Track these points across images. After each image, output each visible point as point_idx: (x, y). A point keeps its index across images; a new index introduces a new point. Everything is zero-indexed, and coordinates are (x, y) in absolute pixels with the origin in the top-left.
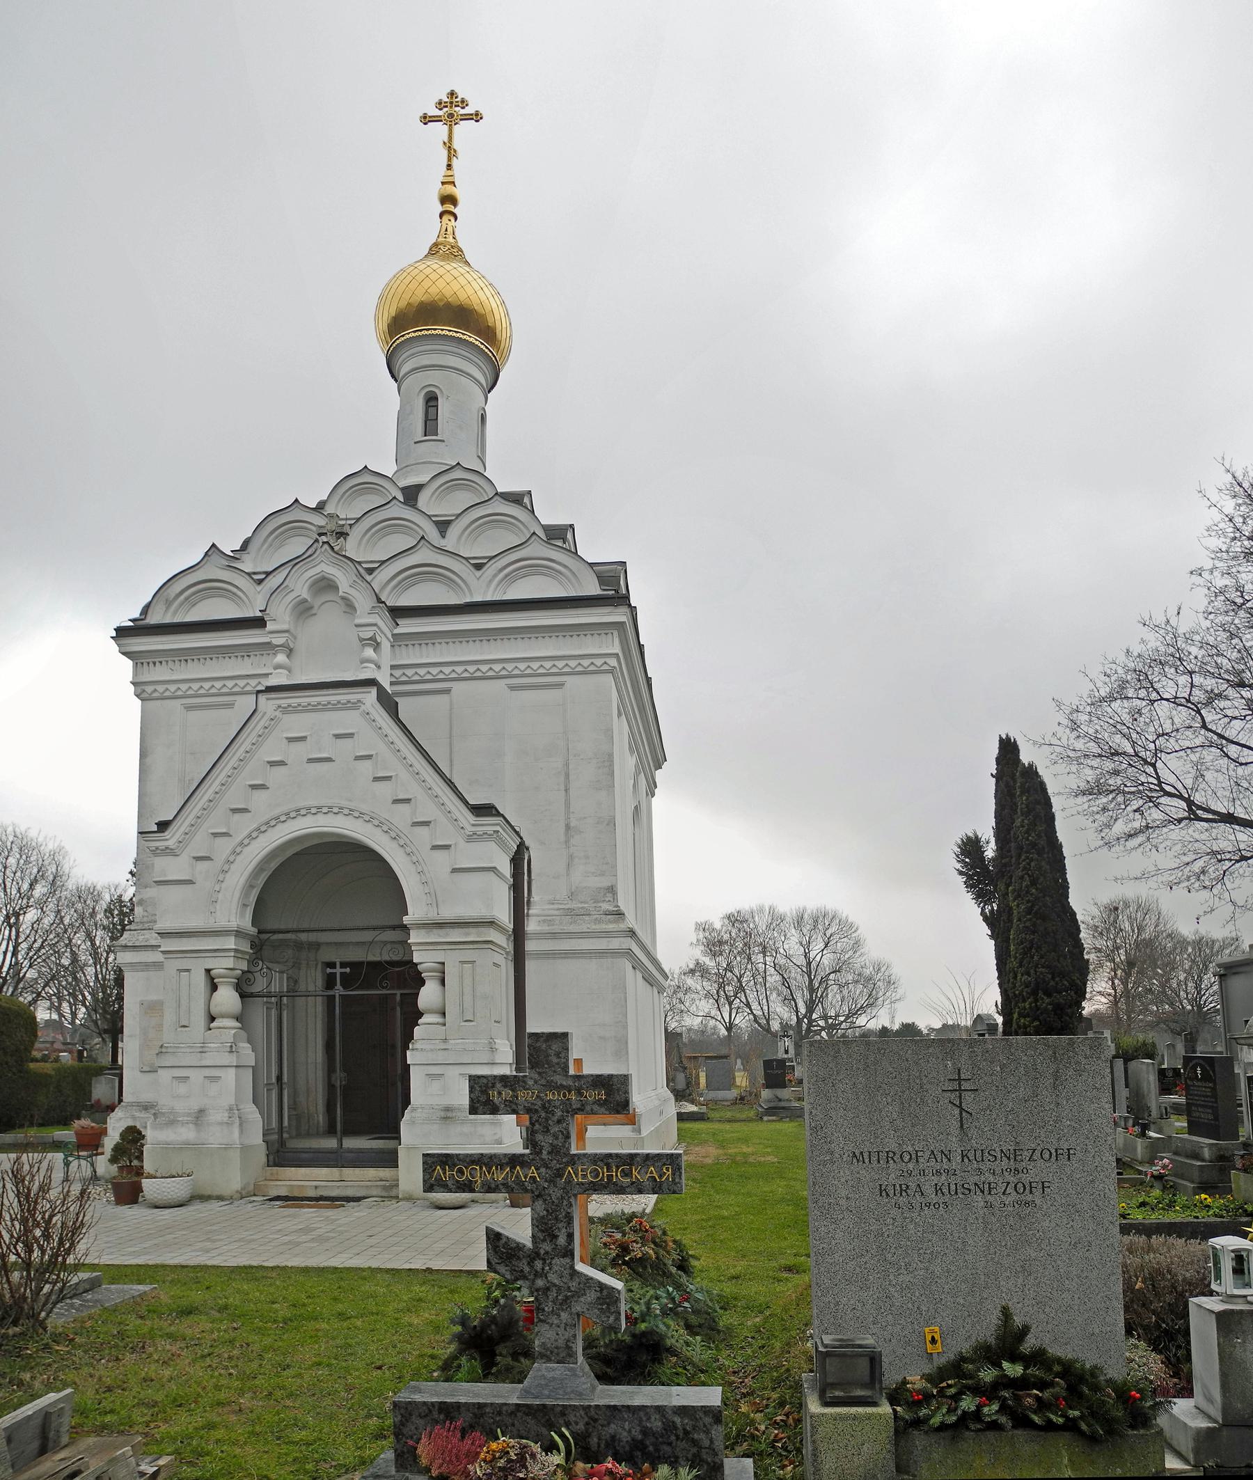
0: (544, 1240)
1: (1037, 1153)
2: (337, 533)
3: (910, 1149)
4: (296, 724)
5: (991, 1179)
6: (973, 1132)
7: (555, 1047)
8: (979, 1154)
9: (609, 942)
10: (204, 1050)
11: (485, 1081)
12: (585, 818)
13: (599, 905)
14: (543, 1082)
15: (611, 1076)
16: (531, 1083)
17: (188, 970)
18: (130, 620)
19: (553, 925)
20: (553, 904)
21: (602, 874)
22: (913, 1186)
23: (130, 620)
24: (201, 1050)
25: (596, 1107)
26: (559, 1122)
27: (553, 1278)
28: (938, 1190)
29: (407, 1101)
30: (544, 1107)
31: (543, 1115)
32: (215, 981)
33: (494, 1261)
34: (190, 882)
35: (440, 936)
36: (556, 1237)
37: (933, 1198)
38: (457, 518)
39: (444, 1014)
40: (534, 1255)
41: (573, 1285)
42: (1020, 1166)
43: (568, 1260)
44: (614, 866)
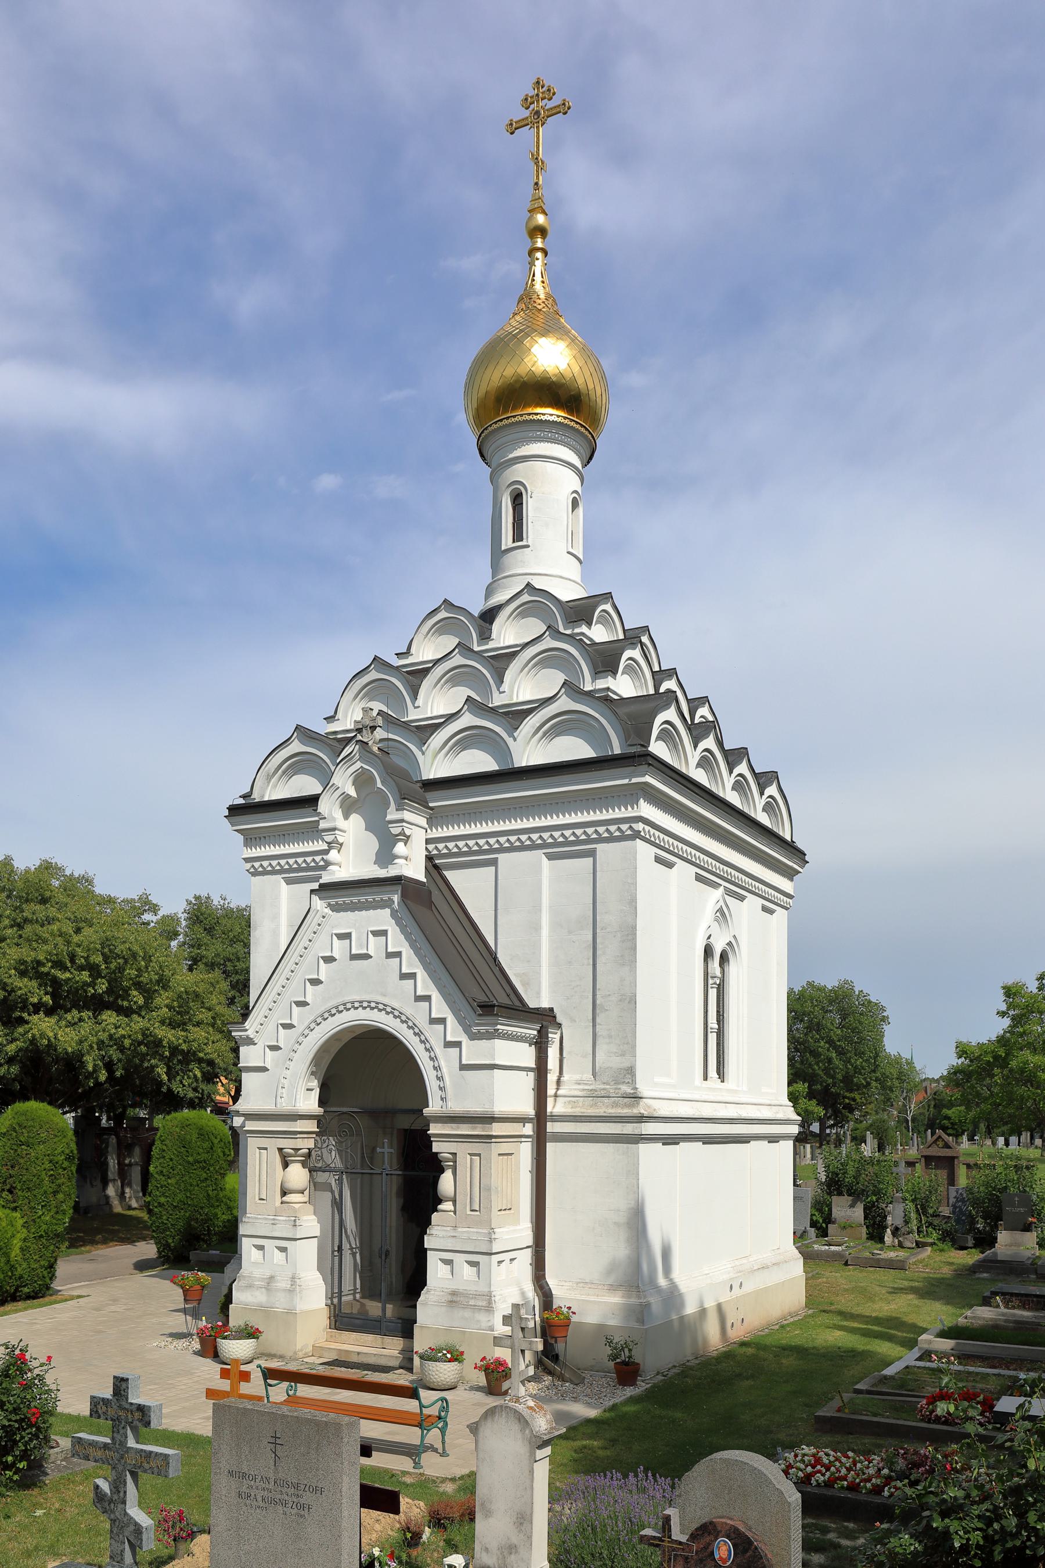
2: (370, 727)
3: (253, 1474)
4: (345, 921)
5: (286, 1498)
6: (280, 1468)
9: (623, 1126)
12: (609, 995)
13: (619, 1086)
14: (118, 1405)
16: (113, 1404)
17: (266, 1149)
18: (240, 797)
20: (579, 1084)
21: (623, 1055)
23: (240, 797)
24: (273, 1222)
29: (426, 1285)
32: (286, 1159)
34: (264, 1069)
36: (119, 1492)
37: (261, 1504)
44: (634, 1047)
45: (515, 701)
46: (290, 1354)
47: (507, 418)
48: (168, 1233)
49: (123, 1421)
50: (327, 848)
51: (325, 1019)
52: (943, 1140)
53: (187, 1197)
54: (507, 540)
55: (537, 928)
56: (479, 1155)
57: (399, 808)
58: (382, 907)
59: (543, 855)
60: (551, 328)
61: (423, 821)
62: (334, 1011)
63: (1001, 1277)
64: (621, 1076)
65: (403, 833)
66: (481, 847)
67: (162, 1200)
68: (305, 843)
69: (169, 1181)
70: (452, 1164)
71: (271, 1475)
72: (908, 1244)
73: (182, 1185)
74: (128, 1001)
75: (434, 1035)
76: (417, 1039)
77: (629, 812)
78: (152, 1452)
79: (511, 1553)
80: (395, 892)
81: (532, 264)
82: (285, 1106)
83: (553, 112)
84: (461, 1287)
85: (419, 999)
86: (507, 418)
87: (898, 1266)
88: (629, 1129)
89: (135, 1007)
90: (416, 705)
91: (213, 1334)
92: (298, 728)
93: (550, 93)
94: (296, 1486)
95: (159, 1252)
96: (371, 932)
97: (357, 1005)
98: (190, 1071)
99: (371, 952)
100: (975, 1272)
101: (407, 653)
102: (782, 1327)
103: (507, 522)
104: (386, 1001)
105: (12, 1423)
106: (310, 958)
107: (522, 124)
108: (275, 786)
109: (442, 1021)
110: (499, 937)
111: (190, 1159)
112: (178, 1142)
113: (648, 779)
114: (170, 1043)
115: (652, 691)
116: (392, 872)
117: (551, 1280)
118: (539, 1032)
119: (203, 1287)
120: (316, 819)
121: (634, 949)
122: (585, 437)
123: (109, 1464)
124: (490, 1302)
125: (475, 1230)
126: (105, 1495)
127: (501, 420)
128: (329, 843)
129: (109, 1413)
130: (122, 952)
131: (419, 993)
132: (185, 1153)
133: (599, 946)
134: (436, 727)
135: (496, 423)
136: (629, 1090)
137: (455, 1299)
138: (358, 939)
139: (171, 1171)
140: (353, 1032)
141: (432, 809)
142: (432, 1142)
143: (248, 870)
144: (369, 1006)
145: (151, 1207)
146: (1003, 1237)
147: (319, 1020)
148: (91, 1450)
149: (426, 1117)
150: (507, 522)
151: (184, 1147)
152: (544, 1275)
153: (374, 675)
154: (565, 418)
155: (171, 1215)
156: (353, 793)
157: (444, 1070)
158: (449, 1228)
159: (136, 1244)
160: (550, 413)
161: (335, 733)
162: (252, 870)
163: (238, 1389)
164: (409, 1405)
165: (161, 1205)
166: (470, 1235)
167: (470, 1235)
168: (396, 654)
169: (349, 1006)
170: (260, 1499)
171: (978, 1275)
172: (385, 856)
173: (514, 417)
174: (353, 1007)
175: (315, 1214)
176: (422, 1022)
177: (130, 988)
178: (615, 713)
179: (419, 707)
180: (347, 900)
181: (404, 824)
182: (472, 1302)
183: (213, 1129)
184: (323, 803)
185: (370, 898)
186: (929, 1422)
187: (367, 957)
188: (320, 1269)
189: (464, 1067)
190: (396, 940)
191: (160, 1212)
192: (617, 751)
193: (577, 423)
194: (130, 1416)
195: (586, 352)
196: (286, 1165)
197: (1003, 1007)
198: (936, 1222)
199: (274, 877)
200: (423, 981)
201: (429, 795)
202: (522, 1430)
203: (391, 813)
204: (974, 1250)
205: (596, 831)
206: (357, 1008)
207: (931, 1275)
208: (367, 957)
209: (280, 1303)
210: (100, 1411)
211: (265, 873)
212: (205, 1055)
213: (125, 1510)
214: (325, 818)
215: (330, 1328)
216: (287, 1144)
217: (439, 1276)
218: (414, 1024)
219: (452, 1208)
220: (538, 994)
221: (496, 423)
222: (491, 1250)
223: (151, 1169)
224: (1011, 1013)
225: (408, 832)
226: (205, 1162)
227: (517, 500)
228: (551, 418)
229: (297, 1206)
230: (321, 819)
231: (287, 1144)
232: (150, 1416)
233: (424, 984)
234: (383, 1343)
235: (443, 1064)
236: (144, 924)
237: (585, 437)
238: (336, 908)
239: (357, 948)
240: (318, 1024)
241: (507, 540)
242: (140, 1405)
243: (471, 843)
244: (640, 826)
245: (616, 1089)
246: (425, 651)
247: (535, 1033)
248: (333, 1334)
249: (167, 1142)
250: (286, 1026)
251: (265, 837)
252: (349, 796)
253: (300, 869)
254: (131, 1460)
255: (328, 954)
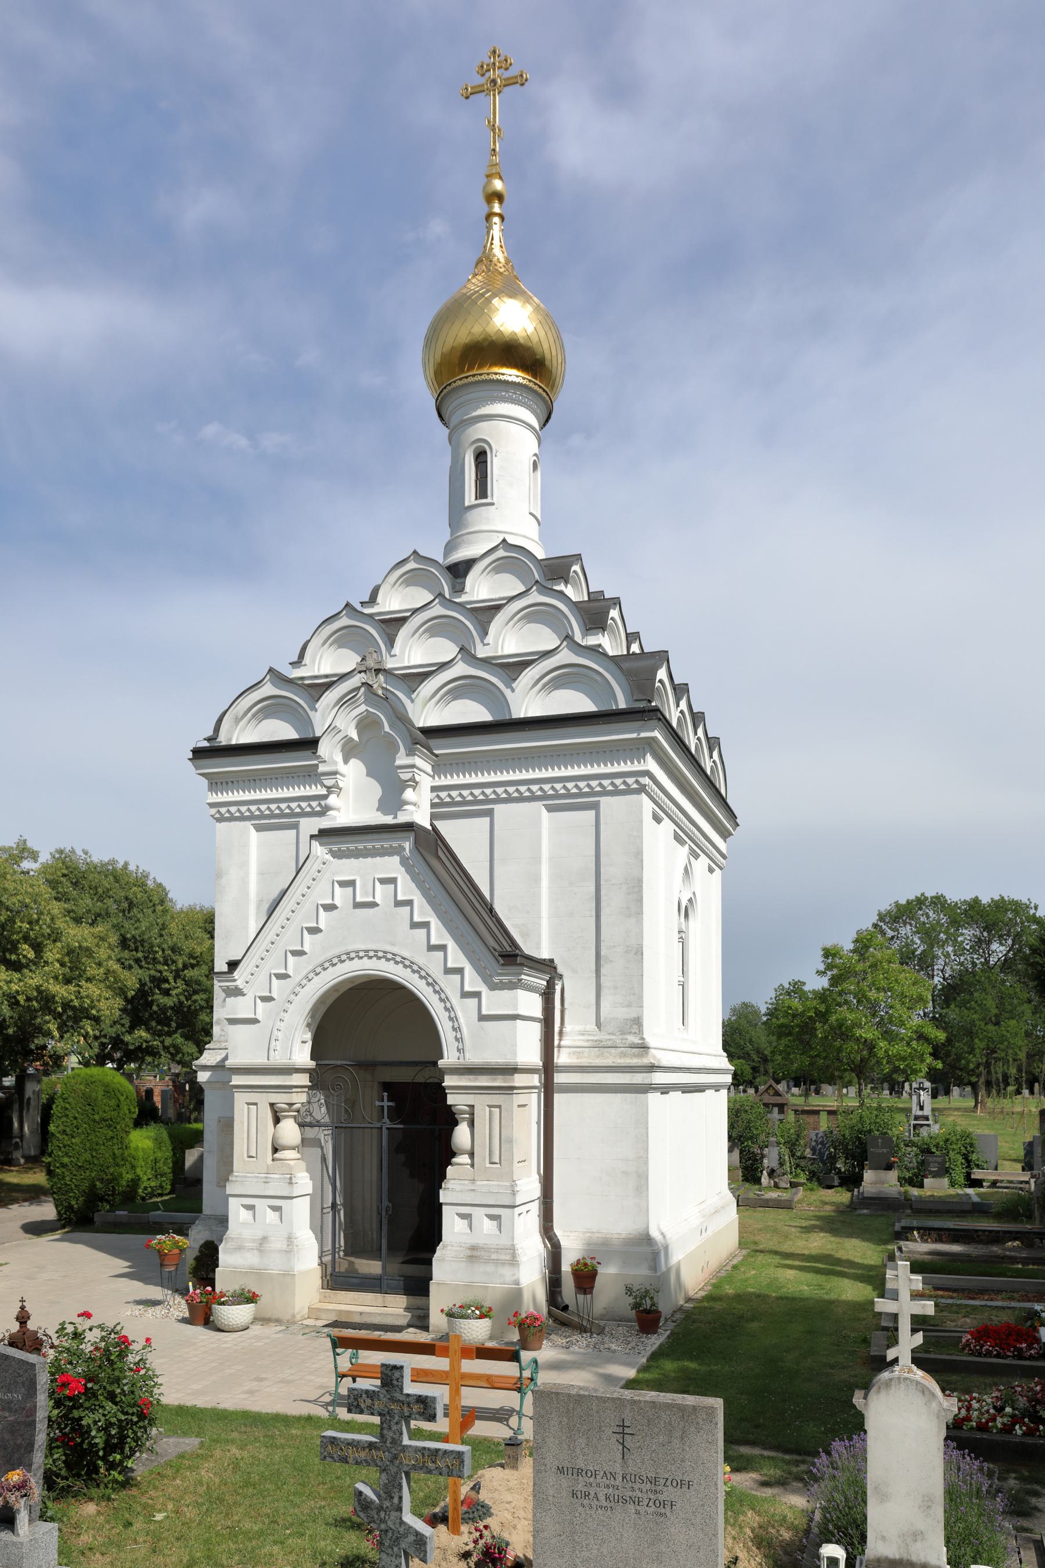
0: (386, 1499)
1: (669, 1482)
3: (592, 1469)
5: (640, 1495)
6: (630, 1462)
7: (397, 1374)
8: (633, 1477)
10: (268, 1180)
11: (356, 1392)
12: (614, 946)
14: (389, 1396)
15: (427, 1397)
16: (382, 1396)
17: (256, 1104)
18: (205, 739)
19: (582, 1058)
20: (583, 1035)
21: (629, 1006)
22: (592, 1494)
23: (205, 739)
24: (265, 1180)
25: (417, 1416)
26: (397, 1423)
27: (390, 1524)
28: (607, 1498)
29: (440, 1240)
30: (388, 1413)
31: (388, 1418)
33: (358, 1509)
34: (254, 1021)
35: (470, 1080)
36: (392, 1498)
38: (507, 603)
39: (473, 1154)
40: (380, 1508)
41: (401, 1529)
42: (659, 1488)
43: (399, 1514)
45: (500, 653)
46: (288, 1317)
47: (474, 376)
48: (71, 1194)
49: (396, 1416)
50: (326, 793)
51: (325, 969)
52: (774, 1089)
53: (93, 1157)
54: (470, 497)
55: (537, 879)
56: (499, 1107)
57: (410, 753)
58: (391, 854)
59: (543, 807)
60: (512, 290)
61: (428, 768)
62: (335, 961)
63: (880, 1213)
64: (628, 1027)
65: (413, 779)
66: (476, 797)
67: (66, 1160)
68: (224, 793)
69: (74, 1141)
70: (467, 1116)
71: (618, 1469)
72: (782, 1185)
73: (88, 1145)
74: (16, 954)
75: (450, 985)
76: (431, 989)
77: (636, 767)
78: (439, 1450)
79: (916, 1541)
80: (407, 839)
81: (489, 228)
82: (278, 1059)
83: (510, 82)
84: (480, 1241)
85: (432, 948)
86: (474, 376)
87: (785, 1205)
88: (638, 1078)
89: (24, 961)
90: (392, 653)
91: (205, 1300)
92: (271, 670)
93: (506, 65)
94: (654, 1481)
95: (59, 1213)
96: (378, 879)
97: (361, 954)
98: (81, 1028)
99: (378, 900)
100: (856, 1209)
101: (373, 599)
102: (735, 1267)
103: (470, 479)
104: (395, 950)
105: (130, 1417)
106: (308, 906)
107: (478, 90)
108: (243, 729)
109: (460, 971)
110: (496, 887)
111: (97, 1117)
112: (82, 1100)
113: (656, 734)
114: (63, 998)
115: (625, 653)
116: (402, 818)
117: (558, 1231)
118: (548, 982)
119: (181, 1250)
120: (316, 762)
121: (640, 901)
122: (543, 399)
123: (377, 1466)
124: (514, 1255)
125: (495, 1183)
126: (372, 1502)
127: (467, 377)
128: (328, 788)
129: (376, 1407)
130: (14, 904)
131: (433, 942)
132: (90, 1111)
133: (603, 898)
134: (328, 686)
135: (461, 379)
136: (637, 1041)
137: (474, 1254)
138: (363, 886)
139: (75, 1130)
140: (353, 982)
141: (437, 756)
142: (446, 1094)
143: (212, 816)
144: (357, 956)
145: (52, 1168)
146: (868, 1175)
147: (319, 970)
148: (350, 1452)
149: (440, 1069)
150: (470, 479)
151: (89, 1105)
152: (552, 1226)
153: (344, 621)
154: (530, 381)
155: (75, 1175)
156: (354, 736)
157: (462, 1020)
158: (466, 1182)
159: (10, 1207)
160: (512, 374)
161: (302, 678)
162: (217, 816)
163: (459, 1367)
164: (506, 1369)
165: (63, 1165)
166: (489, 1188)
167: (489, 1188)
168: (361, 603)
169: (353, 955)
170: (602, 1497)
171: (859, 1212)
172: (392, 799)
173: (481, 375)
174: (357, 956)
175: (307, 1171)
176: (436, 972)
177: (18, 942)
178: (620, 668)
179: (395, 655)
180: (352, 846)
181: (415, 770)
182: (494, 1256)
183: (118, 1086)
184: (324, 745)
185: (378, 845)
186: (980, 1355)
187: (373, 905)
188: (312, 1228)
189: (482, 1018)
190: (407, 888)
191: (63, 1173)
192: (622, 705)
193: (540, 387)
194: (406, 1409)
195: (547, 317)
196: (277, 1120)
197: (822, 967)
198: (803, 1163)
199: (242, 823)
200: (438, 930)
201: (432, 742)
202: (927, 1403)
203: (400, 759)
204: (839, 1189)
205: (517, 790)
206: (361, 958)
207: (817, 1214)
208: (373, 905)
209: (275, 1265)
210: (363, 1406)
211: (232, 819)
212: (98, 1012)
213: (401, 1518)
214: (325, 761)
215: (322, 1288)
216: (280, 1099)
217: (456, 1231)
218: (427, 974)
219: (469, 1161)
220: (538, 946)
221: (461, 379)
222: (515, 1202)
223: (52, 1128)
224: (829, 973)
225: (417, 778)
226: (112, 1120)
227: (481, 458)
228: (510, 379)
229: (292, 1163)
230: (320, 762)
231: (280, 1099)
232: (435, 1409)
233: (438, 933)
234: (384, 1301)
235: (460, 1014)
236: (23, 872)
237: (543, 399)
238: (337, 855)
239: (362, 896)
240: (317, 974)
241: (470, 497)
242: (420, 1396)
243: (465, 793)
244: (646, 780)
245: (622, 1039)
246: (392, 602)
247: (545, 983)
248: (327, 1295)
249: (71, 1100)
250: (280, 977)
251: (232, 782)
252: (351, 739)
253: (272, 816)
254: (408, 1461)
255: (329, 901)
